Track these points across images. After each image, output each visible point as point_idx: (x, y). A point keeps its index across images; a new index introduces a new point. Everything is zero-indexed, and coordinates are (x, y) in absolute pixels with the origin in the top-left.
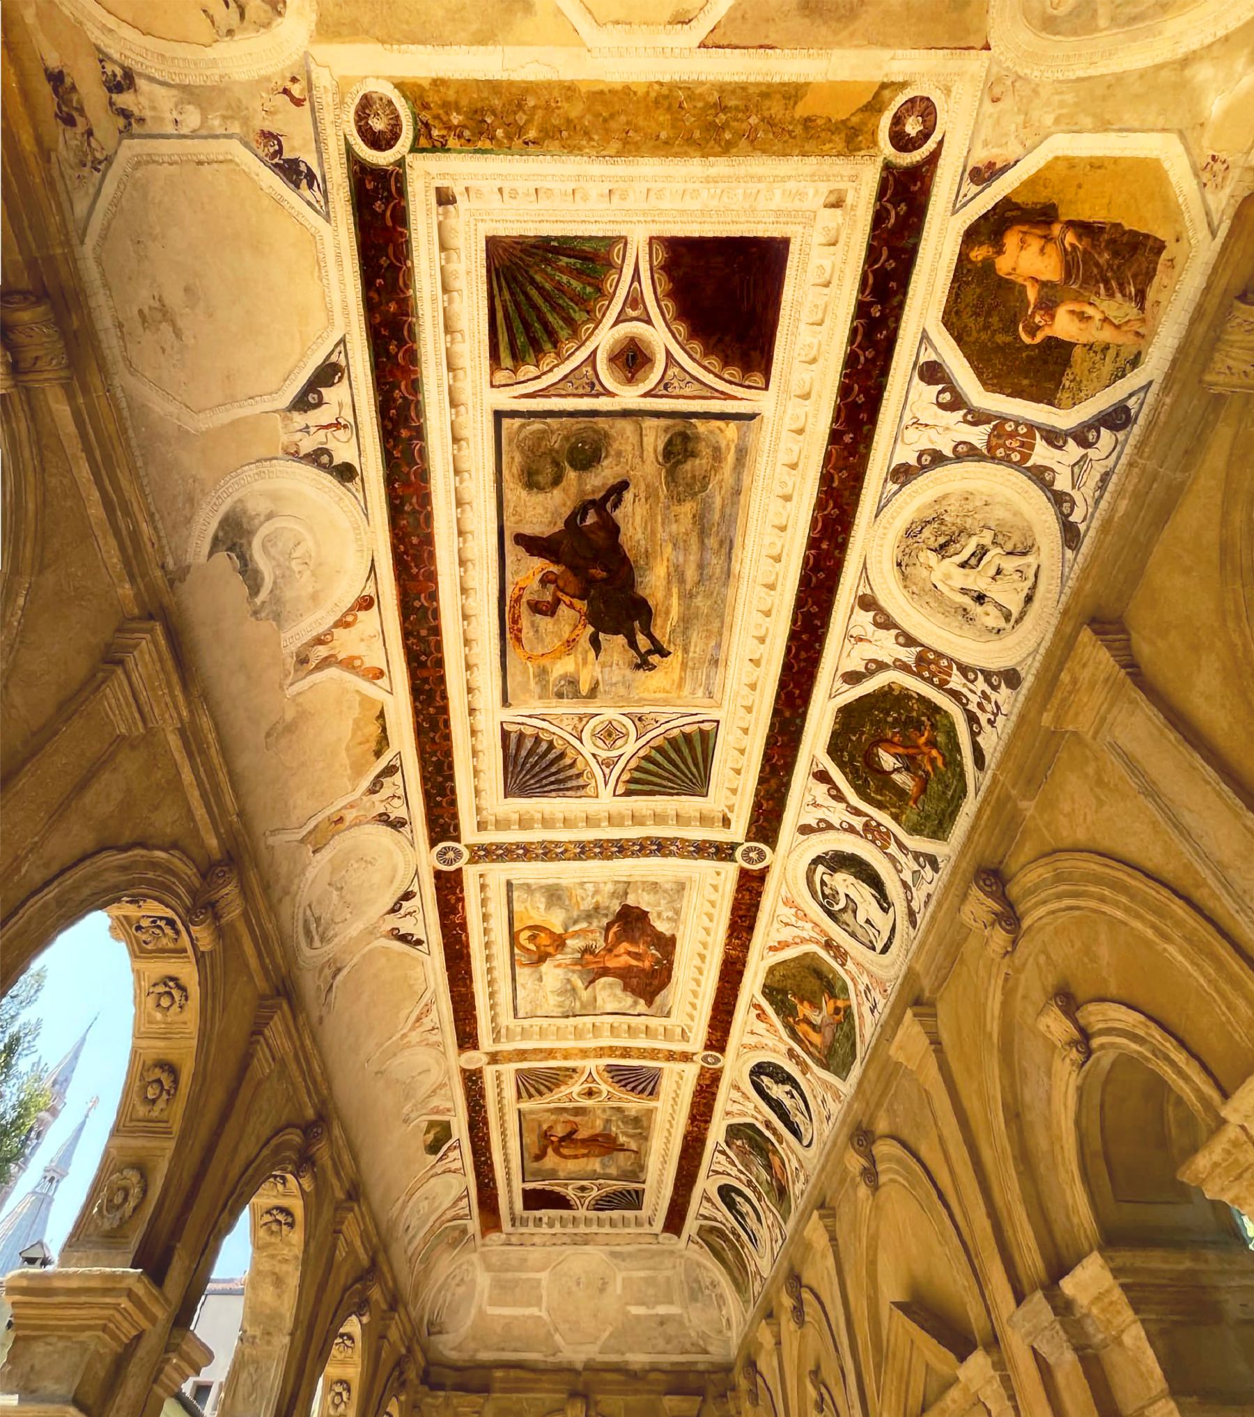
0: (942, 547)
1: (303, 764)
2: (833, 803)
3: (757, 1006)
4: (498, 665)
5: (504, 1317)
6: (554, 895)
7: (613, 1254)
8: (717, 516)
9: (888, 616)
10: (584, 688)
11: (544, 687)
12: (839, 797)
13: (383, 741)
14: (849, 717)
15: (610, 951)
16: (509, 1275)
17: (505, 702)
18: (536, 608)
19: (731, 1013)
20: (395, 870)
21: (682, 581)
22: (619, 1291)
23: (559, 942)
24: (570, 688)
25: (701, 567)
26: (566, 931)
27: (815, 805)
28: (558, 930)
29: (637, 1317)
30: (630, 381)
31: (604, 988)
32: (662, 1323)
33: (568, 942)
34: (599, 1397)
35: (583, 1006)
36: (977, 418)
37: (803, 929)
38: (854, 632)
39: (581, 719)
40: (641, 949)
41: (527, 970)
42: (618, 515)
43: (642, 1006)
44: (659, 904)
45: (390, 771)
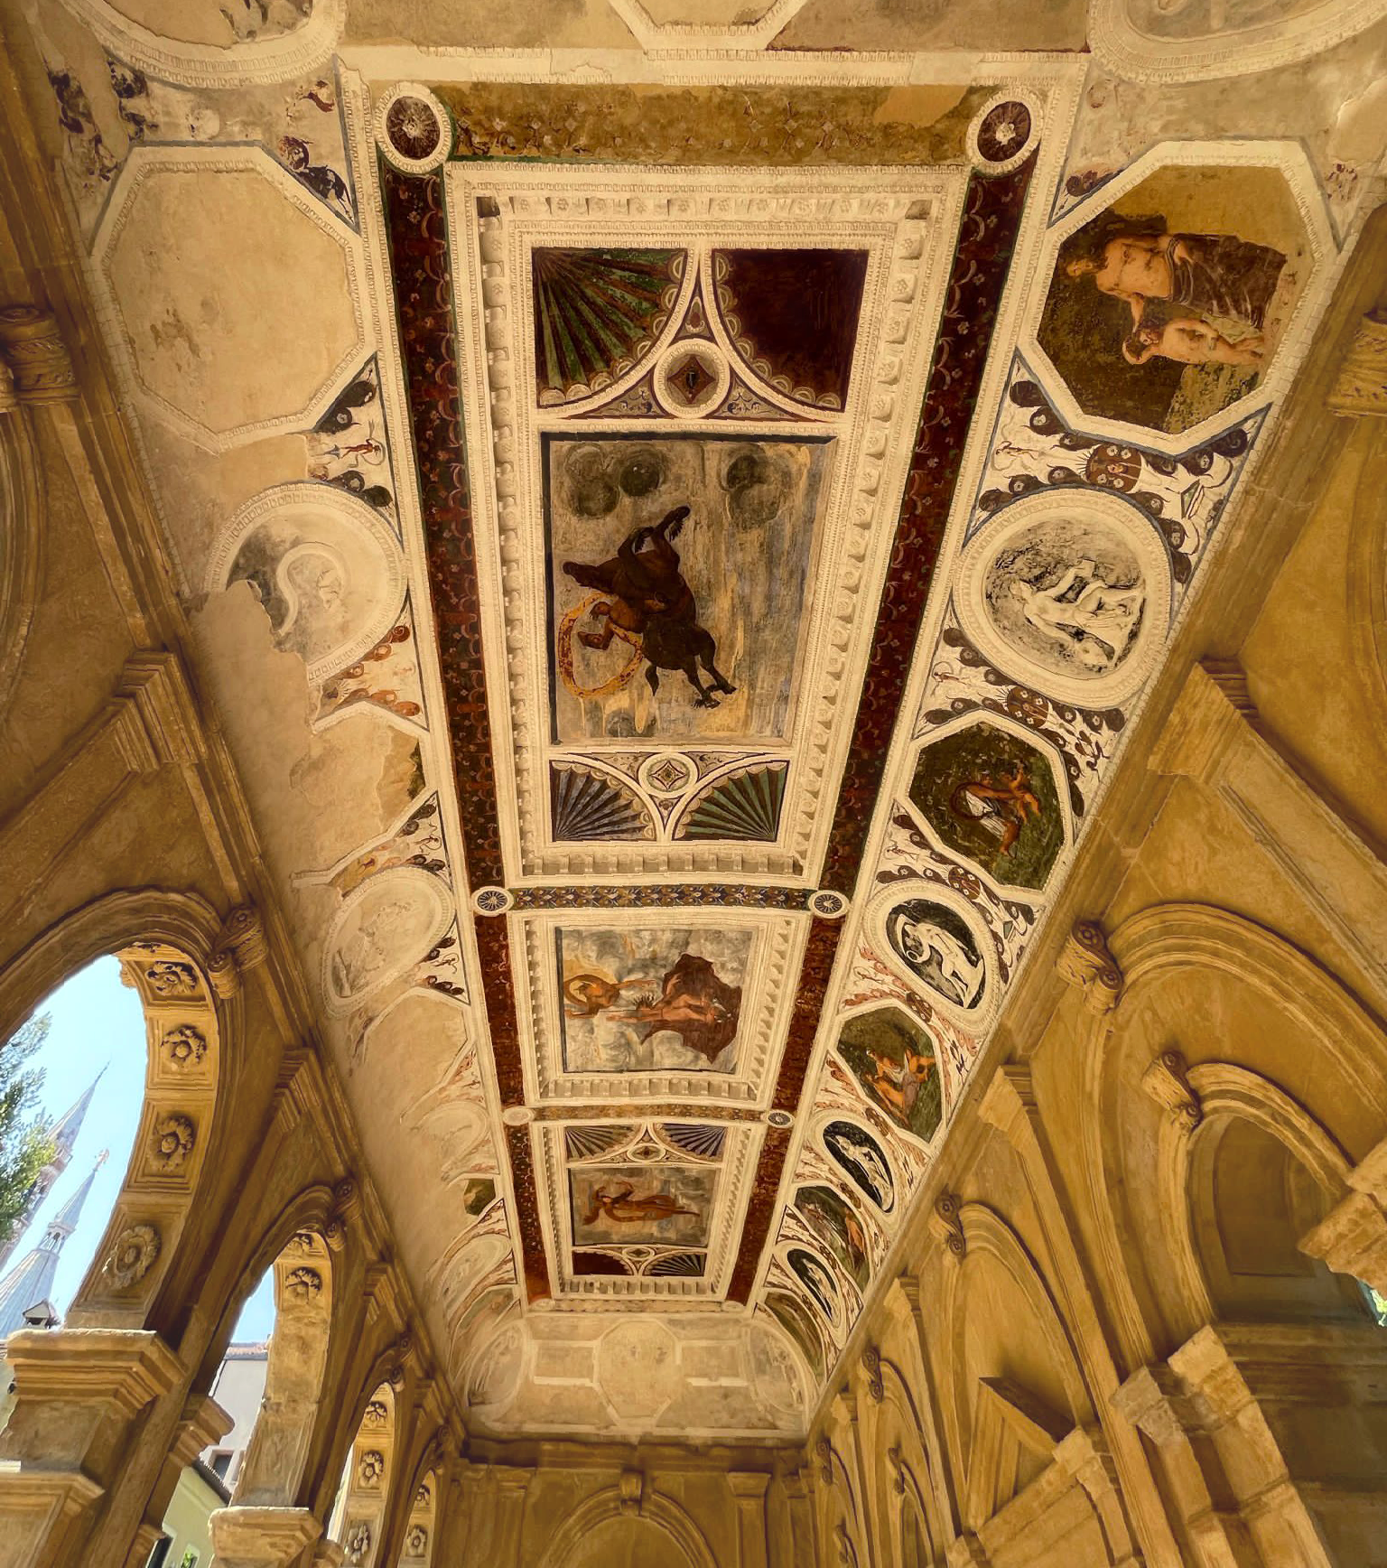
0: (1038, 578)
1: (331, 803)
2: (916, 849)
3: (833, 1064)
4: (547, 700)
5: (553, 1387)
6: (606, 942)
7: (672, 1322)
8: (786, 546)
9: (977, 652)
10: (640, 726)
11: (597, 723)
12: (923, 843)
13: (419, 780)
14: (933, 758)
15: (668, 1003)
16: (559, 1343)
17: (555, 739)
18: (587, 640)
19: (803, 1070)
20: (431, 915)
21: (748, 612)
22: (678, 1362)
23: (613, 993)
24: (624, 726)
25: (769, 598)
26: (620, 981)
27: (897, 851)
29: (699, 1389)
30: (691, 401)
31: (661, 1042)
32: (726, 1396)
33: (623, 992)
34: (656, 1473)
35: (639, 1061)
36: (1075, 442)
37: (883, 982)
38: (939, 670)
39: (636, 759)
40: (703, 1002)
41: (577, 1022)
42: (677, 543)
43: (703, 1061)
44: (722, 955)
45: (426, 811)
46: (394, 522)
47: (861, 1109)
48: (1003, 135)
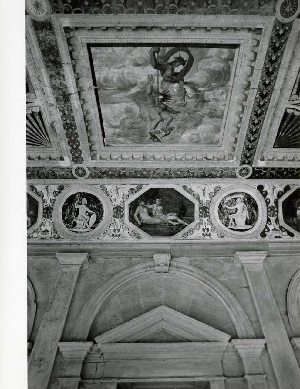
6: (221, 77)
26: (186, 83)
27: (274, 189)
28: (186, 79)
33: (176, 85)
36: (276, 202)
47: (117, 203)
48: (80, 171)
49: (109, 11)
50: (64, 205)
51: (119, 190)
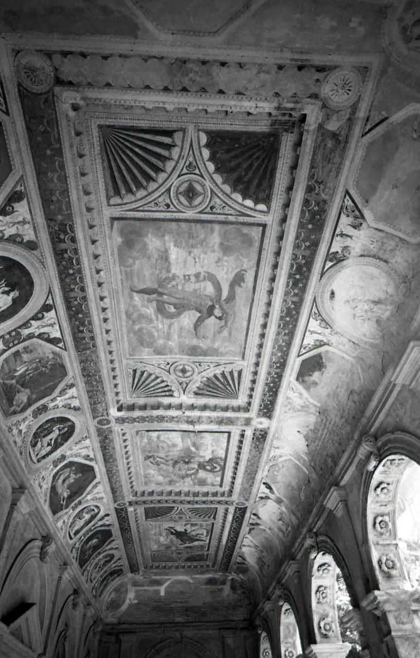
1: (377, 303)
2: (42, 330)
3: (91, 460)
23: (202, 466)
33: (196, 467)
46: (368, 128)
49: (278, 334)
50: (54, 418)
51: (51, 327)
